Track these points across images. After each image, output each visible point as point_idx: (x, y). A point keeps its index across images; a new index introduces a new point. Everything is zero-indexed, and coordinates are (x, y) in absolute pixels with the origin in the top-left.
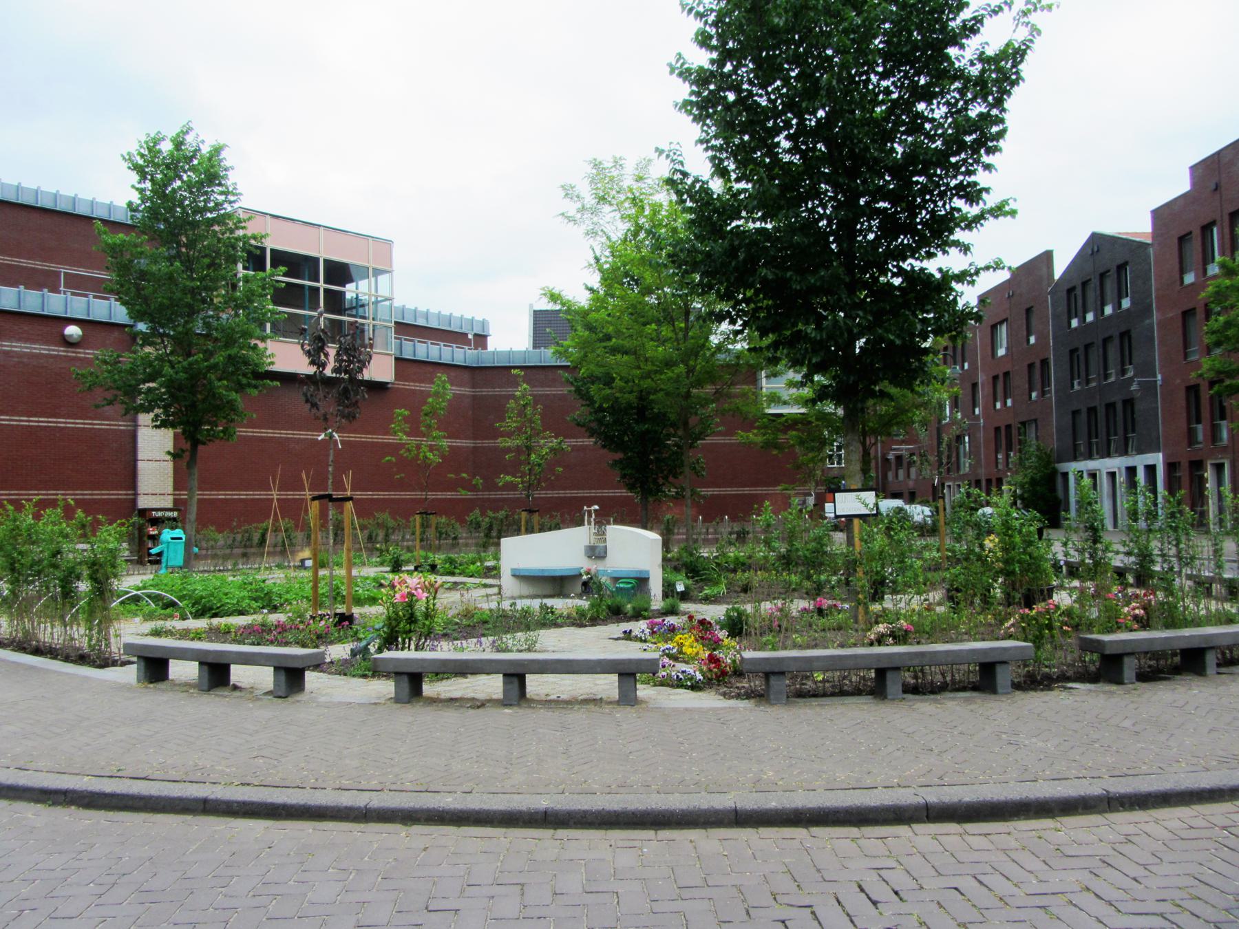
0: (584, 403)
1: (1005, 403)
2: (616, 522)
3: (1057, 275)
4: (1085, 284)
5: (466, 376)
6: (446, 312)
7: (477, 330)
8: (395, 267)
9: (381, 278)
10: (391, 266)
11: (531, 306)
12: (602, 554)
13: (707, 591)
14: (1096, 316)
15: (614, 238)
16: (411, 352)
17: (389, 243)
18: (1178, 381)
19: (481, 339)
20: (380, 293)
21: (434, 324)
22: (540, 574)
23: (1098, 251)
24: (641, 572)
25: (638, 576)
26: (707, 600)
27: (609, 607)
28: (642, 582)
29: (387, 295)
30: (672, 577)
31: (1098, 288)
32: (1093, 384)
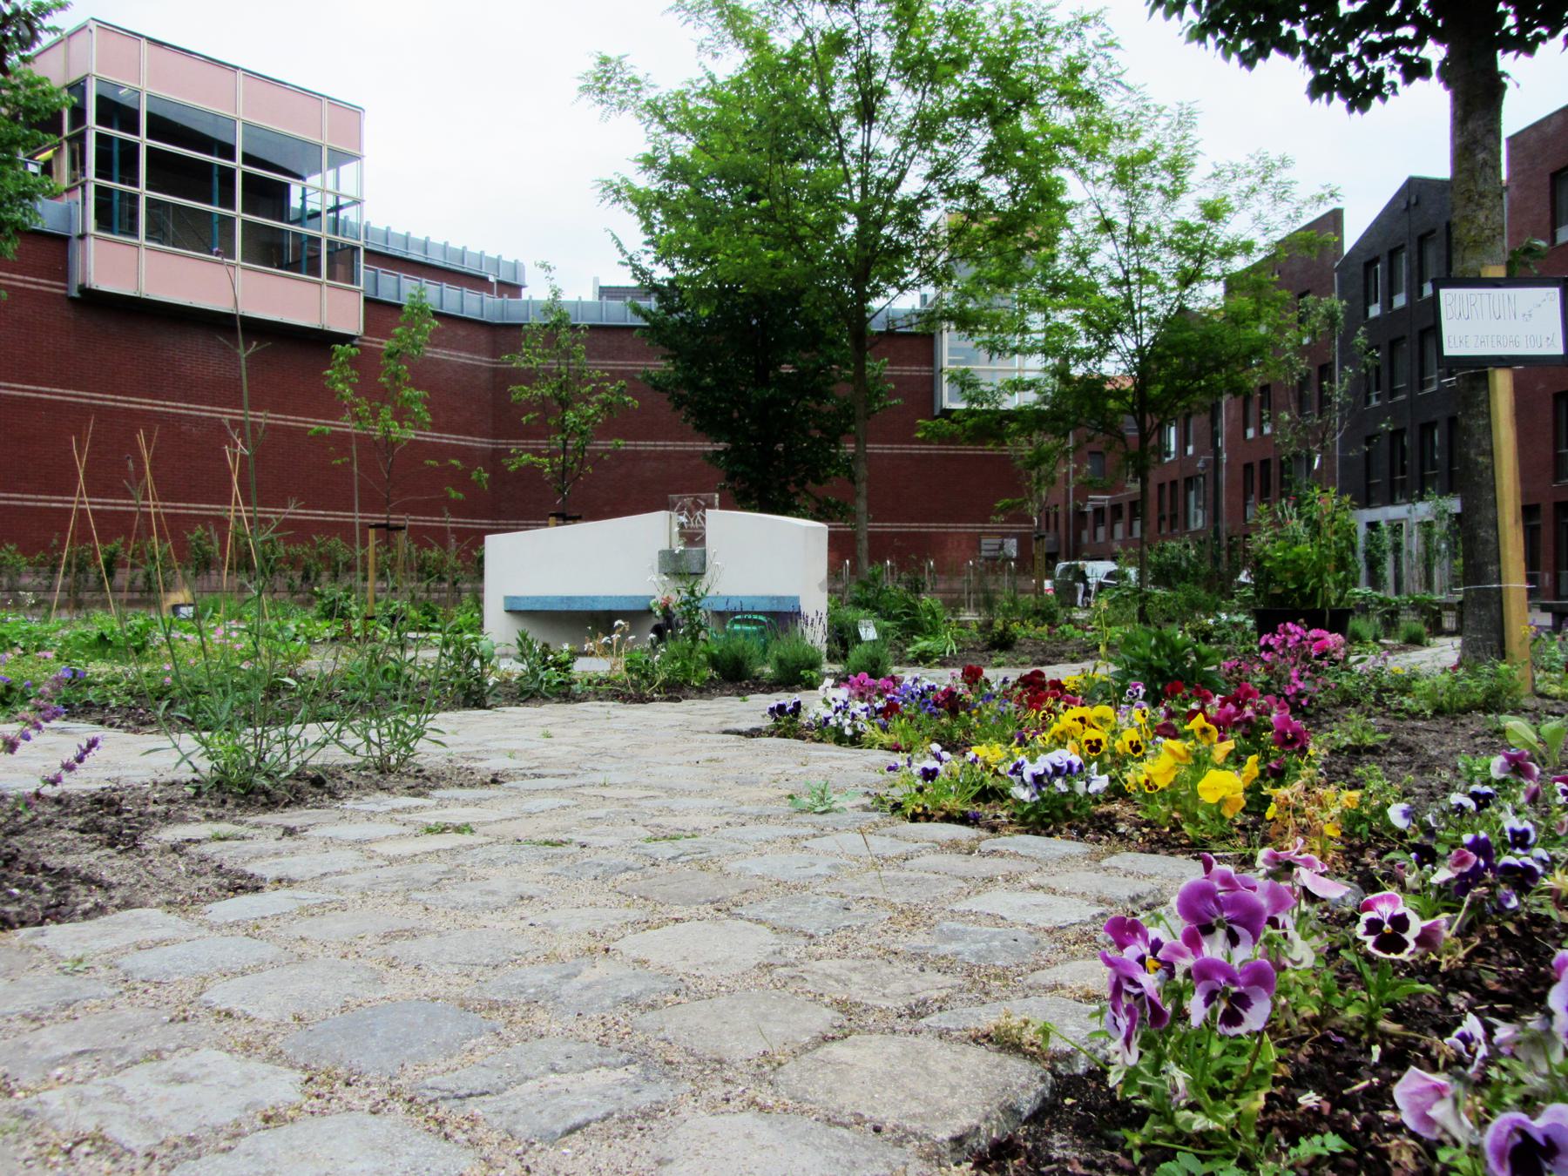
0: (667, 352)
1: (1261, 430)
2: (724, 505)
3: (1347, 248)
4: (1393, 254)
5: (483, 337)
6: (457, 244)
7: (506, 277)
8: (368, 148)
9: (343, 169)
10: (360, 148)
11: (596, 280)
12: (696, 569)
13: (923, 644)
14: (1409, 298)
15: (720, 79)
16: (394, 293)
17: (357, 111)
18: (1541, 386)
19: (512, 289)
20: (342, 191)
21: (437, 259)
22: (564, 608)
23: (1417, 203)
24: (780, 599)
25: (775, 608)
26: (923, 658)
27: (714, 661)
28: (783, 618)
29: (354, 193)
30: (849, 614)
31: (1415, 258)
32: (1402, 397)
